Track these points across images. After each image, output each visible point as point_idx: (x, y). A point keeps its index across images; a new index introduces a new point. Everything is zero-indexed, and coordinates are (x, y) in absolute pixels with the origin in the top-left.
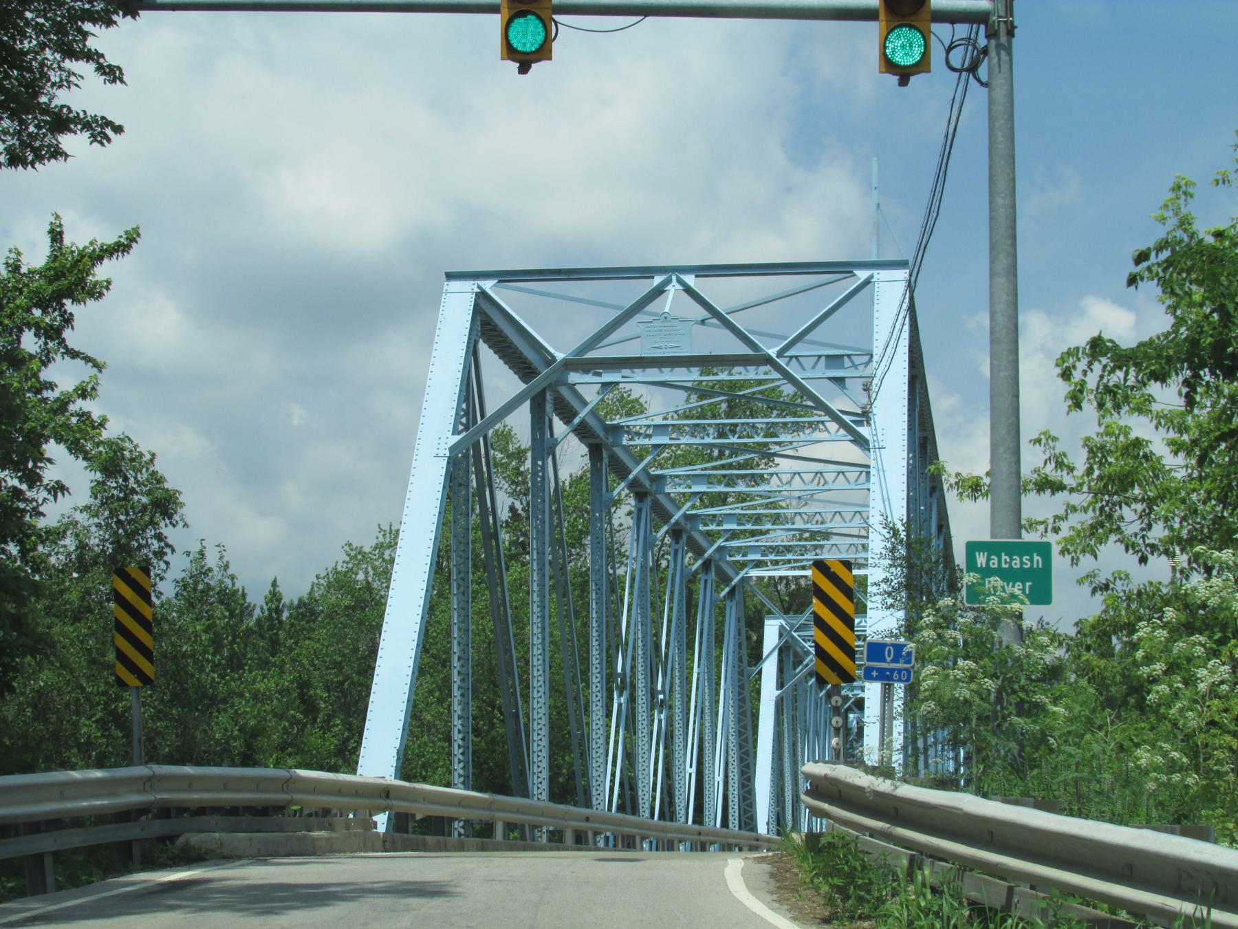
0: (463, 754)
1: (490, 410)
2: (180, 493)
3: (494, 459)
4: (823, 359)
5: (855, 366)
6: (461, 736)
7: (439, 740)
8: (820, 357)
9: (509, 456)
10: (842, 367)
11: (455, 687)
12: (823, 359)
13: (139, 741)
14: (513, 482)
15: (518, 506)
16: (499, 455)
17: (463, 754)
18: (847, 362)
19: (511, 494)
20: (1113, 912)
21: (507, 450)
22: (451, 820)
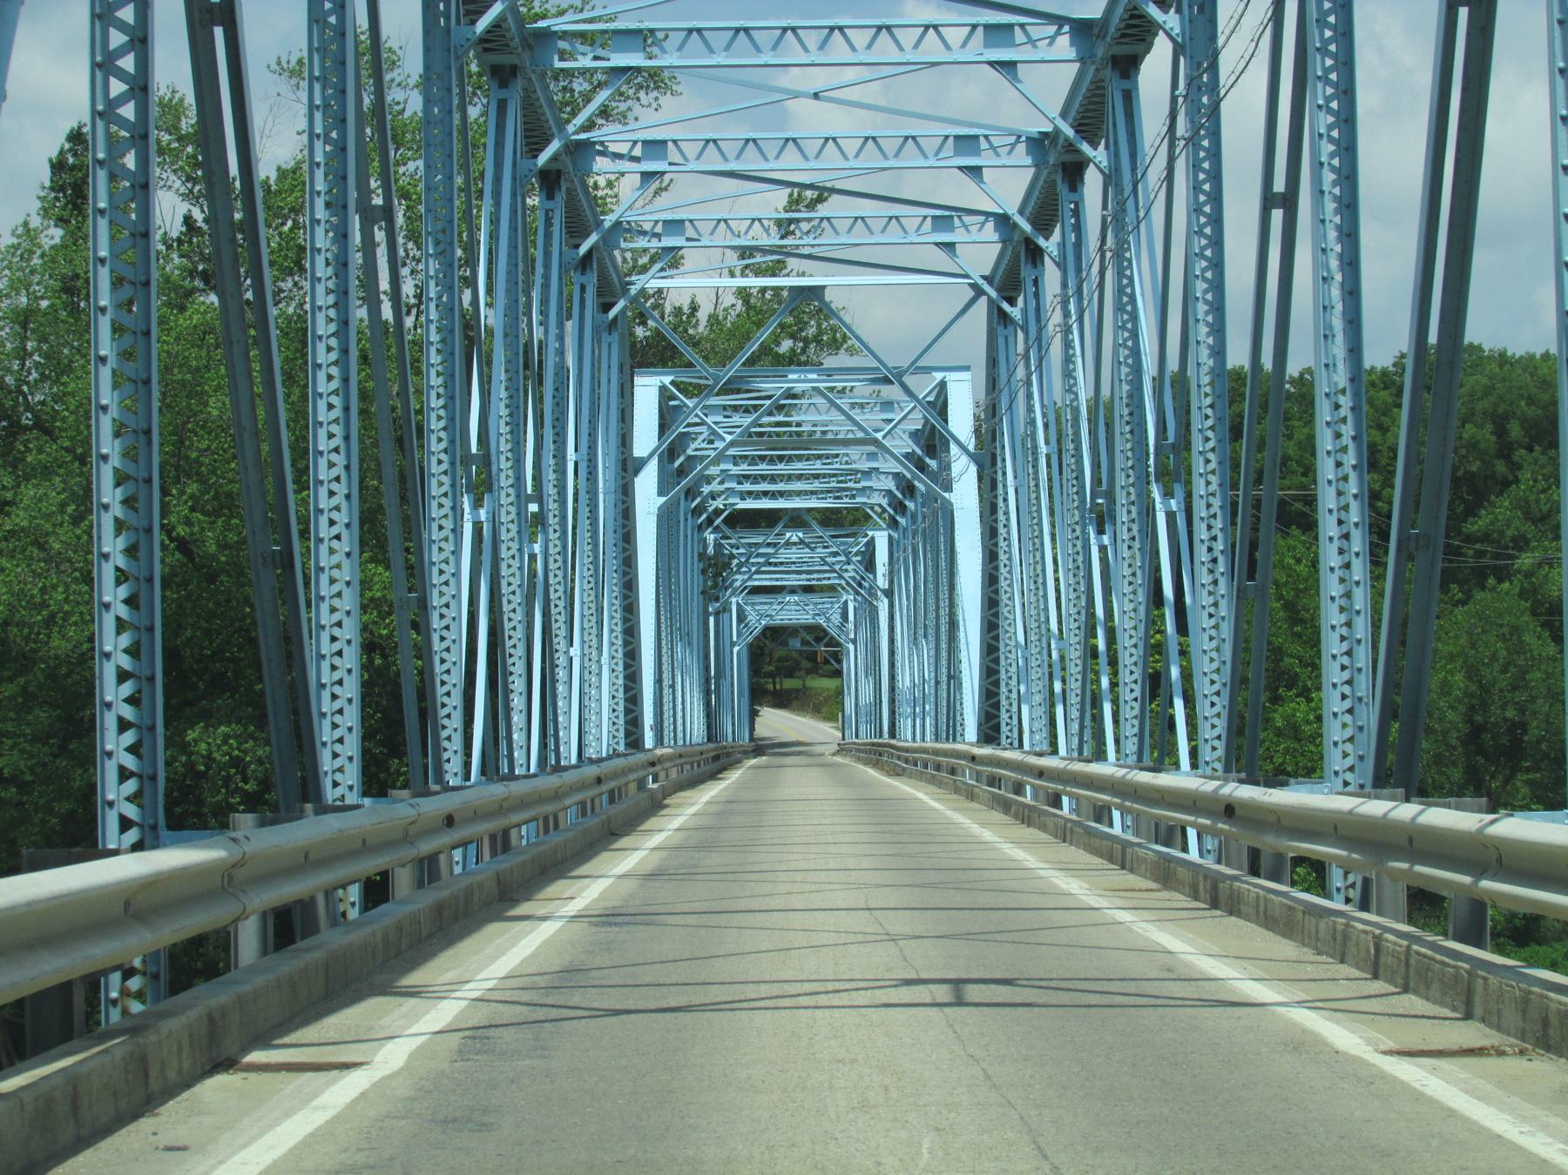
0: (132, 700)
1: (112, 79)
2: (51, 161)
3: (158, 142)
4: (980, 30)
5: (1032, 42)
6: (125, 640)
7: (76, 580)
8: (974, 27)
9: (180, 139)
10: (1012, 44)
11: (106, 477)
12: (980, 30)
13: (596, 58)
14: (189, 178)
15: (198, 215)
16: (165, 137)
17: (132, 700)
18: (1019, 36)
19: (186, 197)
20: (318, 165)
21: (177, 129)
22: (93, 983)
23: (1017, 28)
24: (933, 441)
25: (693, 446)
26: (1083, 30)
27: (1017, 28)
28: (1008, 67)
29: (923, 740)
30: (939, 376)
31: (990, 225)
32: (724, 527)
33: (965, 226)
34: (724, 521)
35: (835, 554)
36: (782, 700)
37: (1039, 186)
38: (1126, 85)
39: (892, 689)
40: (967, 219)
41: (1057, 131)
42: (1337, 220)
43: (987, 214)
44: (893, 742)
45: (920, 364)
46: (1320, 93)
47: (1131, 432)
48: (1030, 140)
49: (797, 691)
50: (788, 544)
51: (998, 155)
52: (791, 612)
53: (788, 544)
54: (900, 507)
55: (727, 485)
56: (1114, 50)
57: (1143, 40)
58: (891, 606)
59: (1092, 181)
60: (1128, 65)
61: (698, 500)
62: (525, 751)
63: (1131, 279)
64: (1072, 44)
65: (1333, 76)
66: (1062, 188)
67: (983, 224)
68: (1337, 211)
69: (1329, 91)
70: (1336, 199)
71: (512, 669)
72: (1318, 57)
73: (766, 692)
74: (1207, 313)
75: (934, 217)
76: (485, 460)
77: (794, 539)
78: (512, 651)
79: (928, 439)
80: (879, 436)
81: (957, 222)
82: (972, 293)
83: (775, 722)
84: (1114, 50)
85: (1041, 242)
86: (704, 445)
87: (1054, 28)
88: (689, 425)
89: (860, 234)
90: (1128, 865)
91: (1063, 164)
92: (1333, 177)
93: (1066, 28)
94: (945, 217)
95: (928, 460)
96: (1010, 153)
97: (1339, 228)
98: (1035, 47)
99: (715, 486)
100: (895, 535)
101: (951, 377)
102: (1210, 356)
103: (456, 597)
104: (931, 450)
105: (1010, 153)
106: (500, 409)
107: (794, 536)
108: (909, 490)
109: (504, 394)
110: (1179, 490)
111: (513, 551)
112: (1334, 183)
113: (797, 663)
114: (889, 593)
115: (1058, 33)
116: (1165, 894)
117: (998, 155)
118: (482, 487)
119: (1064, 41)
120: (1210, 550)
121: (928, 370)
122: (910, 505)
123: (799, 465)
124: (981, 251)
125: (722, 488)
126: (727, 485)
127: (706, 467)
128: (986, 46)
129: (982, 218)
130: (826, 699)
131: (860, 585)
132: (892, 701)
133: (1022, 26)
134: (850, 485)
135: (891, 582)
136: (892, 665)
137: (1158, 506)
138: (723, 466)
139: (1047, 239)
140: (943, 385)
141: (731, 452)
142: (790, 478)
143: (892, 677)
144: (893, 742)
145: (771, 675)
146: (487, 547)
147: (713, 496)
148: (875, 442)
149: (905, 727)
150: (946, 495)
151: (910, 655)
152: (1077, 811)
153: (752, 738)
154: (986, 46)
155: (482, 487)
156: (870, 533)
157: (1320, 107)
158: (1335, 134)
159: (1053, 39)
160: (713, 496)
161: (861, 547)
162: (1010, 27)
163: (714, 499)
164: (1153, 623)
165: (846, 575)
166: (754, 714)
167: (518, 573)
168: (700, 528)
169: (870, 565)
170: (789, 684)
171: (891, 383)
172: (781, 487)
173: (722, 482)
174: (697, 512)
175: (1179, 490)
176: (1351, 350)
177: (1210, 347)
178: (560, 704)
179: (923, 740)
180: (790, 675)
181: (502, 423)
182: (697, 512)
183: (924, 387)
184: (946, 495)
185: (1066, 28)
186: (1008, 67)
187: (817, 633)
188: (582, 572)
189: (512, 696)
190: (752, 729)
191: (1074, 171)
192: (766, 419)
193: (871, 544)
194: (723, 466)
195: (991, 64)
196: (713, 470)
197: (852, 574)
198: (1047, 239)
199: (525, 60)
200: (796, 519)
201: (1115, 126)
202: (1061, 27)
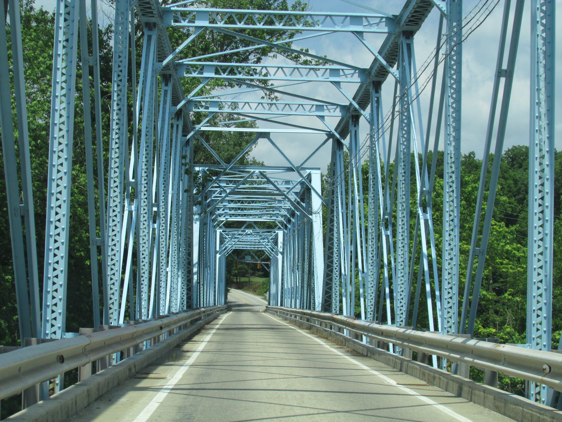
5: (345, 75)
23: (341, 71)
24: (305, 193)
25: (214, 195)
26: (363, 72)
27: (341, 71)
28: (337, 84)
29: (295, 307)
30: (308, 171)
31: (338, 109)
32: (223, 227)
33: (328, 109)
34: (224, 225)
35: (264, 239)
36: (240, 286)
37: (360, 95)
38: (408, 41)
39: (282, 288)
40: (330, 107)
41: (351, 104)
42: (544, 48)
43: (337, 105)
44: (282, 308)
45: (303, 166)
46: (449, 92)
47: (374, 203)
48: (387, 18)
49: (246, 282)
50: (247, 234)
51: (330, 112)
52: (248, 240)
53: (247, 234)
54: (289, 221)
55: (225, 211)
56: (403, 30)
57: (417, 24)
58: (283, 258)
59: (362, 121)
60: (377, 86)
61: (214, 216)
62: (146, 311)
63: (375, 151)
64: (359, 77)
65: (405, 143)
66: (372, 91)
67: (336, 109)
68: (544, 44)
69: (452, 91)
70: (544, 39)
71: (142, 282)
72: (449, 80)
73: (233, 282)
74: (453, 113)
75: (317, 105)
76: (135, 186)
77: (249, 233)
78: (143, 275)
79: (301, 196)
80: (285, 193)
81: (325, 107)
82: (326, 137)
83: (237, 295)
84: (403, 30)
85: (342, 141)
86: (218, 195)
87: (353, 71)
88: (212, 187)
89: (287, 111)
90: (404, 369)
91: (373, 82)
92: (542, 28)
93: (357, 71)
94: (321, 105)
95: (291, 219)
96: (334, 111)
97: (545, 53)
98: (347, 77)
99: (221, 212)
100: (286, 231)
101: (313, 172)
102: (453, 131)
103: (119, 241)
104: (303, 200)
105: (334, 111)
106: (143, 166)
107: (249, 231)
108: (293, 215)
109: (144, 160)
110: (390, 228)
111: (145, 233)
112: (543, 31)
113: (247, 271)
114: (282, 253)
115: (355, 73)
116: (431, 387)
117: (330, 112)
118: (133, 196)
119: (356, 75)
120: (541, 164)
121: (305, 169)
122: (293, 220)
123: (252, 211)
124: (333, 119)
125: (223, 212)
126: (225, 211)
127: (217, 204)
128: (330, 76)
129: (335, 107)
130: (259, 286)
131: (273, 251)
132: (282, 293)
133: (343, 70)
134: (271, 212)
135: (283, 249)
136: (282, 280)
137: (383, 233)
138: (224, 204)
139: (364, 110)
140: (309, 175)
141: (227, 198)
142: (249, 209)
143: (282, 284)
144: (282, 308)
145: (236, 275)
146: (134, 227)
147: (220, 215)
148: (284, 195)
149: (287, 302)
150: (310, 216)
151: (291, 276)
152: (371, 343)
153: (226, 302)
154: (330, 76)
155: (133, 196)
156: (277, 232)
157: (449, 96)
158: (544, 8)
159: (353, 74)
160: (220, 215)
161: (273, 237)
162: (338, 70)
163: (220, 216)
164: (380, 274)
165: (267, 247)
166: (227, 291)
167: (147, 243)
168: (215, 227)
169: (276, 243)
170: (243, 279)
171: (294, 171)
172: (245, 212)
173: (223, 210)
174: (214, 220)
175: (390, 228)
176: (548, 110)
177: (454, 127)
178: (161, 302)
179: (295, 307)
180: (244, 276)
181: (143, 172)
182: (214, 220)
183: (305, 173)
184: (310, 216)
185: (357, 71)
186: (337, 84)
187: (260, 253)
188: (172, 249)
189: (142, 294)
190: (226, 298)
191: (356, 118)
192: (242, 186)
193: (277, 235)
194: (224, 204)
195: (317, 116)
196: (220, 205)
197: (270, 246)
198: (364, 110)
199: (174, 74)
200: (250, 225)
201: (403, 52)
202: (356, 71)
